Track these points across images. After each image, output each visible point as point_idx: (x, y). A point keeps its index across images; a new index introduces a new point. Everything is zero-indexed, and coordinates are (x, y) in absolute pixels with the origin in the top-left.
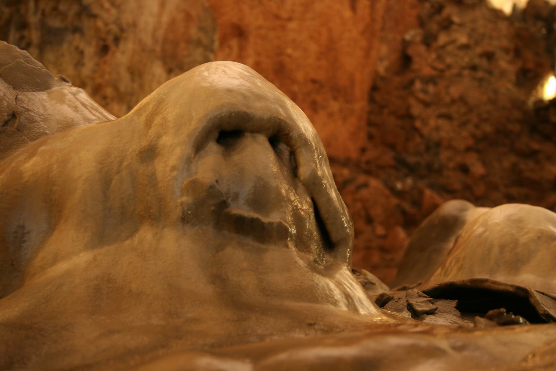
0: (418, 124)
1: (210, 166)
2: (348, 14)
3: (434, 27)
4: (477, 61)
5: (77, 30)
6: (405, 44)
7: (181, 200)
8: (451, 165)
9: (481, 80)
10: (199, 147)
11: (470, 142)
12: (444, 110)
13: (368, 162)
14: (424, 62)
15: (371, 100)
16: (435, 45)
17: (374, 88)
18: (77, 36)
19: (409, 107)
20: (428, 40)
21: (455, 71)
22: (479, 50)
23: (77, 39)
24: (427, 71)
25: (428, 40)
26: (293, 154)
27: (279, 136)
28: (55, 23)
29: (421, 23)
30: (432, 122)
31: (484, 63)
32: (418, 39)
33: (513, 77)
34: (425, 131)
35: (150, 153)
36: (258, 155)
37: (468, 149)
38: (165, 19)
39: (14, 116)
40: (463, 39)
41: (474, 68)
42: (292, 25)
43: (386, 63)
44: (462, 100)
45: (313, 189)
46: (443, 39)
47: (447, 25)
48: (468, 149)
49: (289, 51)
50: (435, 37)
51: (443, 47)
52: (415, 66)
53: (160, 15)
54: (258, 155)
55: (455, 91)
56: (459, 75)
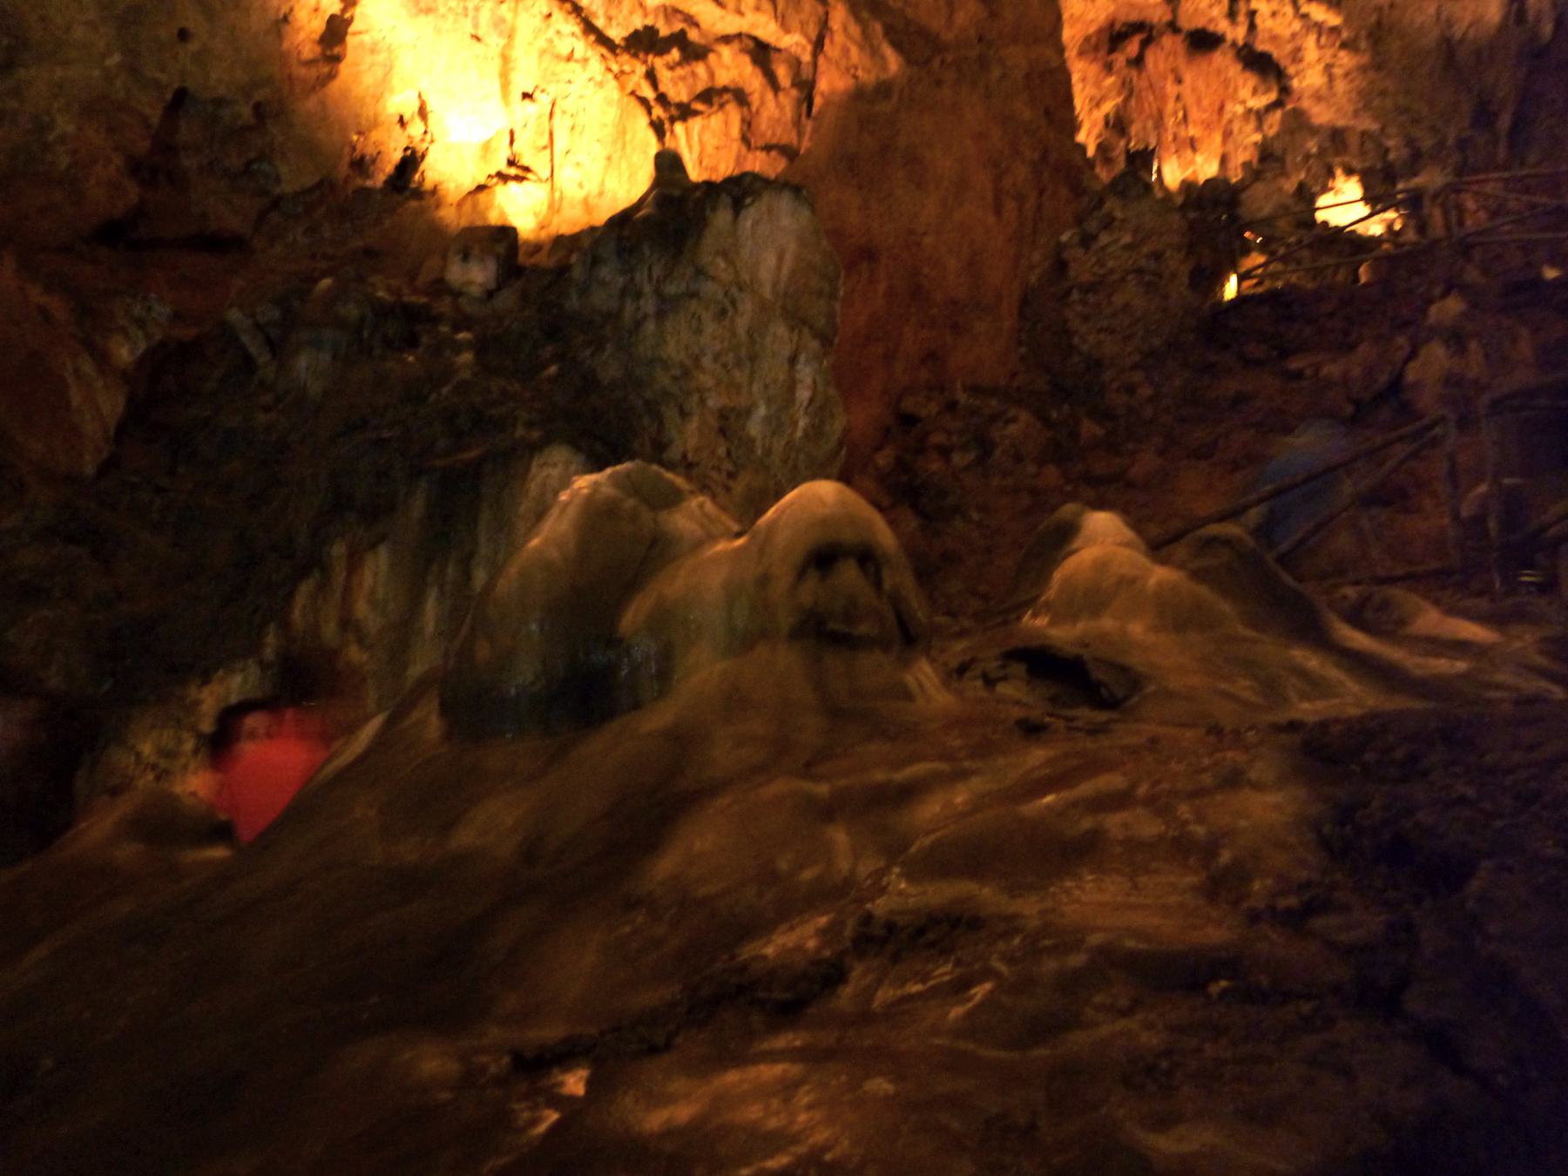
0: (1076, 340)
1: (811, 589)
2: (991, 219)
3: (1092, 225)
4: (1143, 262)
5: (694, 295)
6: (1061, 248)
7: (785, 621)
8: (1115, 385)
9: (1149, 284)
10: (801, 574)
11: (1136, 358)
12: (1105, 323)
13: (1019, 388)
14: (1083, 267)
15: (1021, 315)
16: (1095, 247)
17: (1025, 302)
18: (694, 302)
19: (1065, 321)
20: (1087, 241)
21: (1116, 277)
22: (1145, 250)
23: (694, 305)
24: (1086, 277)
25: (1087, 241)
26: (878, 572)
27: (867, 557)
28: (671, 289)
29: (1079, 221)
30: (1092, 338)
31: (1152, 265)
32: (1076, 239)
33: (1186, 280)
34: (1085, 348)
35: (764, 581)
36: (849, 574)
37: (1135, 367)
38: (785, 271)
39: (654, 542)
40: (1127, 239)
41: (1140, 271)
42: (928, 240)
43: (1038, 271)
44: (1126, 307)
45: (896, 600)
46: (1104, 238)
47: (1108, 223)
48: (1135, 367)
49: (926, 270)
50: (1095, 238)
51: (1103, 248)
52: (1072, 273)
53: (779, 268)
54: (849, 574)
55: (1118, 299)
56: (1123, 279)
